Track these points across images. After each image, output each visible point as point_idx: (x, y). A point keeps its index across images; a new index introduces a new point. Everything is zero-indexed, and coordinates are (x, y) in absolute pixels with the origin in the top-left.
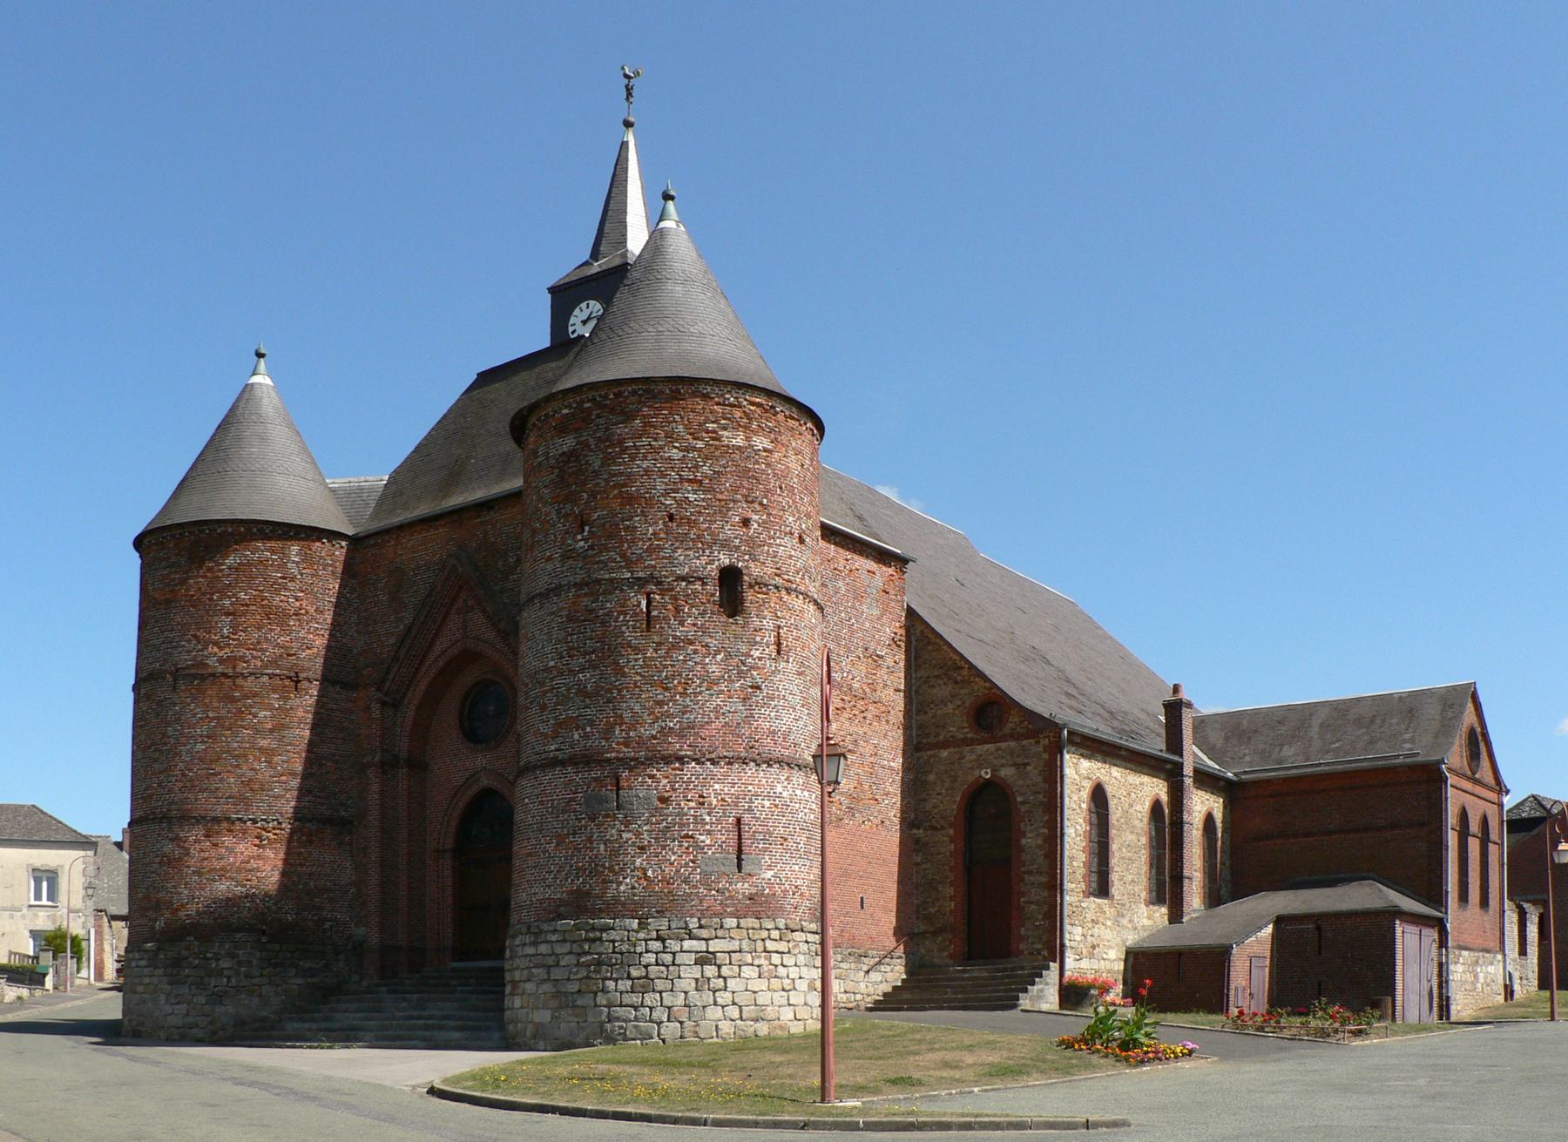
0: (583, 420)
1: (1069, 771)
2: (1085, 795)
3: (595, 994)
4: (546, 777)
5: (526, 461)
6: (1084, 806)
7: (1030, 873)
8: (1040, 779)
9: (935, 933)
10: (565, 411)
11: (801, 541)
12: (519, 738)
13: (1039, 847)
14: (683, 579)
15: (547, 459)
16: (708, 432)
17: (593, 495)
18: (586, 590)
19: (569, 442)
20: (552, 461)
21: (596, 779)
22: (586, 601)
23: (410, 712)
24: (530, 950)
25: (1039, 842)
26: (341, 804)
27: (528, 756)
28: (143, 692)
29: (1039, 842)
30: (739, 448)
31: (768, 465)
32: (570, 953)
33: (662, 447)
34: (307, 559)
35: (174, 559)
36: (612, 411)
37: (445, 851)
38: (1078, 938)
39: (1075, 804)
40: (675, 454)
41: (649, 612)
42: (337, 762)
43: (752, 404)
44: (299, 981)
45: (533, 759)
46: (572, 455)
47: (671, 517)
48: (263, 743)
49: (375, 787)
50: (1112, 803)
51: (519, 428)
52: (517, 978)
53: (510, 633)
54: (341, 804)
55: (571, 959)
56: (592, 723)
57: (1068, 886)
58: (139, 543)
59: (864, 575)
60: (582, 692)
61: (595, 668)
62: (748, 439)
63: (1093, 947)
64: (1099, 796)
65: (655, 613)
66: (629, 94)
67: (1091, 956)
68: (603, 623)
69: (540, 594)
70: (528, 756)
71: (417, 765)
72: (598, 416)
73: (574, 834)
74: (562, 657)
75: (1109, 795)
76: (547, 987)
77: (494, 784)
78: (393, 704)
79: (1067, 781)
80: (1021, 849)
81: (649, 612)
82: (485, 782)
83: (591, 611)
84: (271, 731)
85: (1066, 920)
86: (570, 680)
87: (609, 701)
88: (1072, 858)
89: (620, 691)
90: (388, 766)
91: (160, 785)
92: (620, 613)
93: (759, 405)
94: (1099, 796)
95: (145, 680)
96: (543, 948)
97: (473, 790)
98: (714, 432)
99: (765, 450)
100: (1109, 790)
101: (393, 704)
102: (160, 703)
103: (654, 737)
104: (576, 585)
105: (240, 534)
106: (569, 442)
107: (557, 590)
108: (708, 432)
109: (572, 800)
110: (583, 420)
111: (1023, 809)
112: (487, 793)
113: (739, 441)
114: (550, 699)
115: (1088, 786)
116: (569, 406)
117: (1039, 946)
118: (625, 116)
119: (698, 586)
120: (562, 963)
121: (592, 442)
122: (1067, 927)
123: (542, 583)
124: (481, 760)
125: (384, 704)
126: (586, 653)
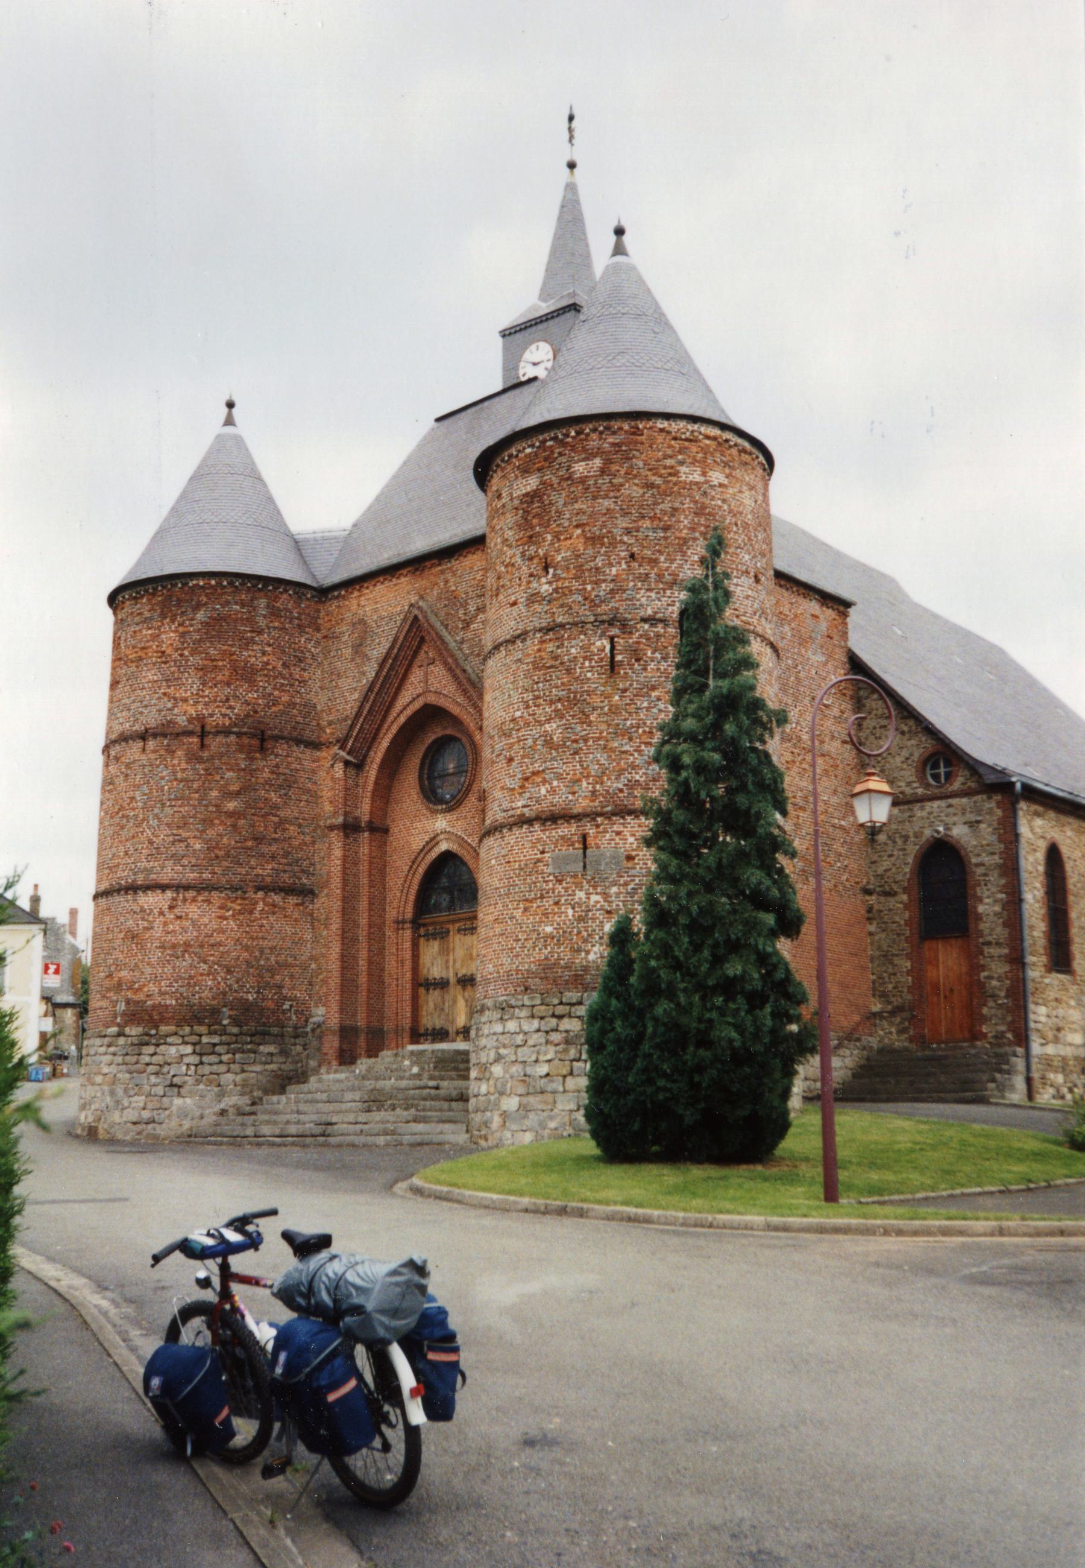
0: (546, 459)
1: (1024, 829)
2: (1041, 856)
3: (565, 1077)
4: (512, 837)
5: (489, 504)
6: (1041, 869)
7: (989, 944)
8: (994, 838)
9: (892, 1013)
10: (528, 450)
11: (757, 580)
12: (483, 797)
13: (996, 914)
14: (644, 620)
15: (512, 500)
16: (665, 467)
17: (557, 537)
18: (551, 635)
19: (532, 483)
20: (516, 502)
21: (562, 837)
22: (550, 647)
23: (372, 771)
24: (498, 1028)
25: (997, 908)
26: (303, 871)
27: (495, 813)
28: (113, 753)
29: (997, 908)
30: (697, 483)
31: (724, 501)
32: (538, 1030)
33: (622, 485)
34: (274, 613)
35: (147, 614)
36: (573, 449)
37: (404, 922)
38: (1043, 1019)
39: (1032, 864)
40: (636, 492)
41: (613, 656)
42: (300, 826)
43: (707, 437)
44: (258, 1068)
45: (500, 816)
46: (532, 497)
47: (632, 556)
48: (231, 805)
49: (338, 853)
50: (1068, 866)
51: (484, 468)
52: (484, 1060)
53: (472, 688)
54: (303, 871)
55: (538, 1038)
56: (559, 777)
57: (1030, 959)
58: (114, 599)
59: (810, 621)
60: (549, 743)
61: (562, 717)
62: (704, 474)
63: (1059, 1030)
64: (1054, 856)
65: (619, 658)
66: (571, 138)
67: (1056, 1040)
68: (568, 671)
69: (507, 641)
70: (495, 813)
71: (379, 830)
72: (561, 454)
73: (542, 897)
74: (528, 707)
75: (1065, 860)
76: (515, 1069)
77: (454, 847)
78: (357, 766)
79: (1023, 841)
80: (979, 917)
81: (613, 656)
82: (444, 846)
83: (556, 658)
84: (238, 793)
85: (1030, 999)
86: (536, 731)
87: (576, 753)
88: (1032, 927)
89: (586, 741)
90: (350, 828)
91: (126, 853)
92: (585, 658)
93: (715, 439)
94: (1054, 856)
95: (124, 738)
96: (512, 1026)
97: (434, 854)
98: (672, 467)
99: (721, 485)
100: (1065, 851)
101: (357, 766)
102: (128, 766)
103: (621, 791)
104: (540, 630)
105: (212, 587)
106: (532, 483)
107: (523, 636)
108: (665, 467)
109: (539, 861)
110: (546, 459)
111: (980, 871)
112: (447, 857)
113: (697, 477)
114: (517, 752)
115: (1043, 845)
116: (532, 446)
117: (1003, 1028)
118: (567, 158)
119: (660, 629)
120: (531, 1042)
121: (555, 481)
122: (1031, 1007)
123: (505, 632)
124: (441, 823)
125: (347, 763)
126: (552, 702)
